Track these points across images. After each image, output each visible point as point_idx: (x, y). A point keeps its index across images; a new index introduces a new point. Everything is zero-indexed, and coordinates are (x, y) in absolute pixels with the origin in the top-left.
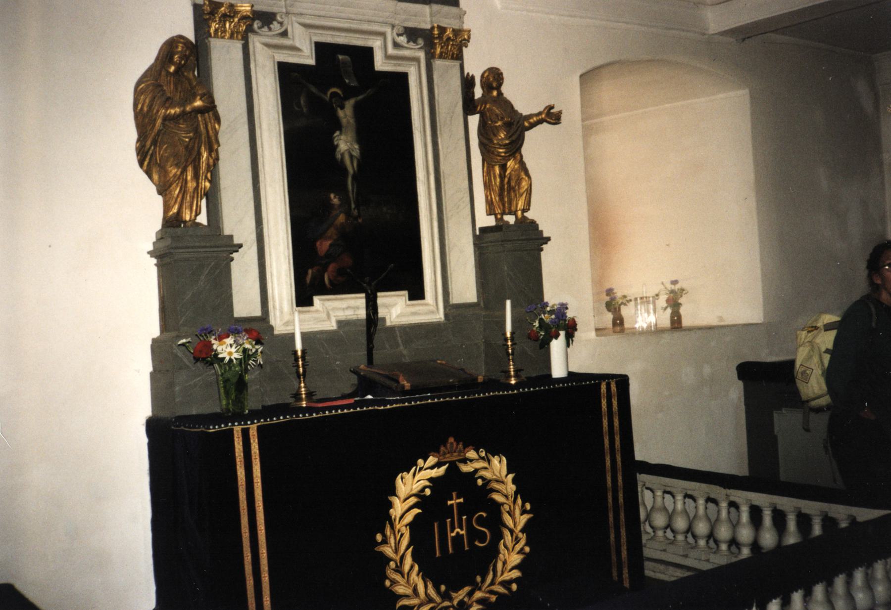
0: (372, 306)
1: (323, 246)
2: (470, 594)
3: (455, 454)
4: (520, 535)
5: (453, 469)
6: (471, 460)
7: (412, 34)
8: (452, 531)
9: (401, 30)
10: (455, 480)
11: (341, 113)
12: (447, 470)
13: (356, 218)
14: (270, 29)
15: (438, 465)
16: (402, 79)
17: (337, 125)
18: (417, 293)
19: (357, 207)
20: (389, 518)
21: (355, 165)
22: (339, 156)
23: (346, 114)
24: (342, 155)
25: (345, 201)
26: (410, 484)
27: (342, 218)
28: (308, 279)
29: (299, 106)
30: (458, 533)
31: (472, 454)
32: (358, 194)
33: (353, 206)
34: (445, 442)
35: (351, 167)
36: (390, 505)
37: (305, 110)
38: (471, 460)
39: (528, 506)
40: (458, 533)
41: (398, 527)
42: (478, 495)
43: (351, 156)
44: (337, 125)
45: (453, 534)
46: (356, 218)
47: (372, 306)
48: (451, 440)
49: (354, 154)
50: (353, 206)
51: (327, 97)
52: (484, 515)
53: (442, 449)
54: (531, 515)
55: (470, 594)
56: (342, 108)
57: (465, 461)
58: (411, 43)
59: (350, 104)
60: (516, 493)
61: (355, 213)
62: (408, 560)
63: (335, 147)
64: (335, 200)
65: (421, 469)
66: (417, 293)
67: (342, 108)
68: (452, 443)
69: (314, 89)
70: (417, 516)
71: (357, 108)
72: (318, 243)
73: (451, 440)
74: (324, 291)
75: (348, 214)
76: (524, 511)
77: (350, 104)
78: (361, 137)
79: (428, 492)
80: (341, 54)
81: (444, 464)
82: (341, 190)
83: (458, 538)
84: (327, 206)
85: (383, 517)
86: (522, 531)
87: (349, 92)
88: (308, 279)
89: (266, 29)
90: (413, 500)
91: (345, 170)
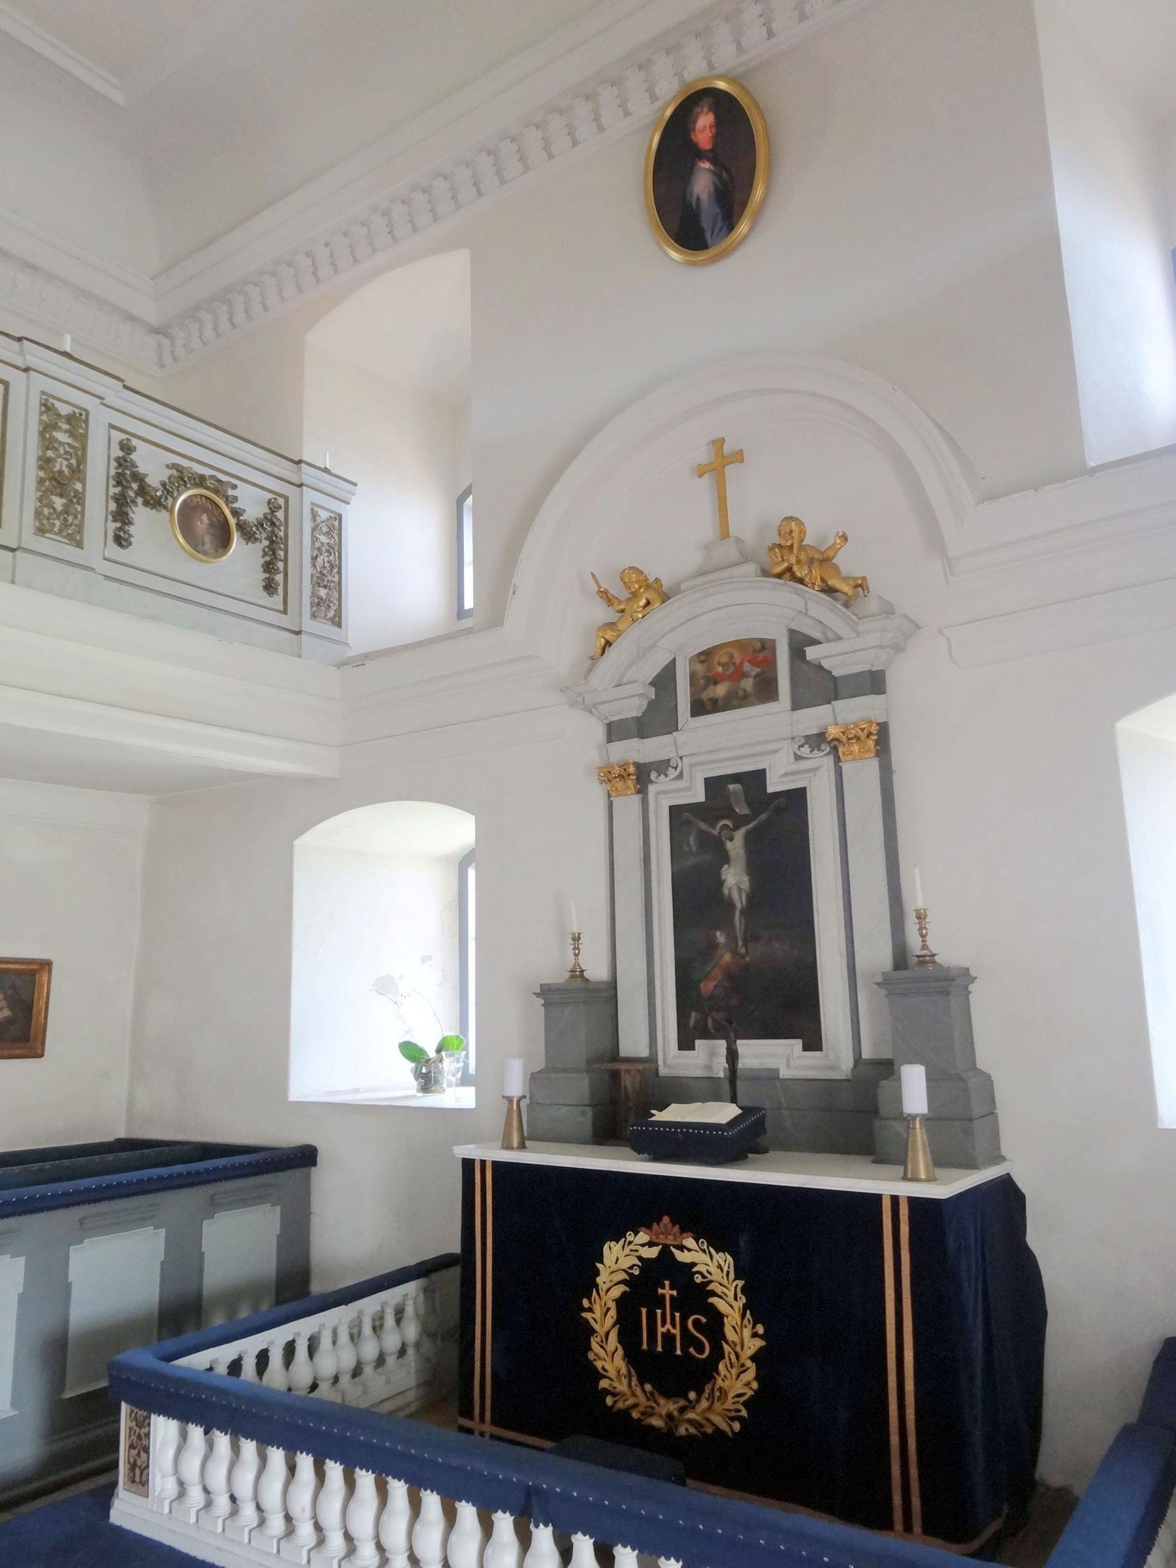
0: (732, 1056)
1: (708, 987)
2: (682, 1410)
3: (671, 1237)
4: (749, 1363)
5: (666, 1253)
6: (689, 1250)
7: (817, 740)
8: (663, 1326)
9: (803, 741)
10: (664, 1267)
11: (729, 845)
12: (660, 1252)
13: (743, 957)
14: (666, 776)
15: (651, 1244)
16: (797, 799)
17: (725, 859)
18: (813, 1042)
19: (745, 944)
20: (597, 1286)
21: (744, 899)
22: (726, 891)
23: (736, 847)
24: (730, 889)
25: (732, 938)
26: (619, 1259)
27: (727, 957)
28: (692, 1022)
29: (688, 845)
30: (668, 1330)
31: (690, 1242)
32: (746, 930)
33: (740, 943)
34: (659, 1221)
35: (739, 901)
36: (597, 1273)
37: (694, 848)
38: (689, 1250)
39: (760, 1329)
40: (668, 1330)
41: (604, 1298)
42: (695, 1295)
43: (740, 890)
44: (725, 859)
45: (664, 1330)
46: (743, 957)
47: (732, 1056)
48: (666, 1219)
49: (742, 887)
50: (740, 943)
51: (716, 832)
52: (704, 1320)
53: (655, 1226)
54: (763, 1343)
55: (682, 1410)
56: (731, 839)
57: (681, 1248)
58: (815, 751)
59: (740, 835)
60: (745, 1307)
61: (743, 951)
62: (613, 1336)
63: (720, 883)
64: (721, 937)
65: (630, 1243)
66: (813, 1042)
67: (731, 839)
68: (665, 1225)
69: (703, 826)
70: (624, 1293)
71: (748, 837)
72: (702, 985)
73: (666, 1219)
74: (706, 1035)
75: (735, 953)
76: (755, 1335)
77: (740, 835)
78: (754, 866)
79: (636, 1272)
80: (732, 783)
81: (657, 1244)
82: (728, 926)
83: (669, 1338)
84: (712, 946)
85: (589, 1285)
86: (753, 1358)
87: (740, 822)
88: (692, 1022)
89: (662, 776)
90: (622, 1276)
91: (733, 906)
